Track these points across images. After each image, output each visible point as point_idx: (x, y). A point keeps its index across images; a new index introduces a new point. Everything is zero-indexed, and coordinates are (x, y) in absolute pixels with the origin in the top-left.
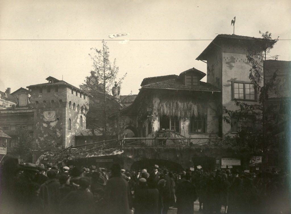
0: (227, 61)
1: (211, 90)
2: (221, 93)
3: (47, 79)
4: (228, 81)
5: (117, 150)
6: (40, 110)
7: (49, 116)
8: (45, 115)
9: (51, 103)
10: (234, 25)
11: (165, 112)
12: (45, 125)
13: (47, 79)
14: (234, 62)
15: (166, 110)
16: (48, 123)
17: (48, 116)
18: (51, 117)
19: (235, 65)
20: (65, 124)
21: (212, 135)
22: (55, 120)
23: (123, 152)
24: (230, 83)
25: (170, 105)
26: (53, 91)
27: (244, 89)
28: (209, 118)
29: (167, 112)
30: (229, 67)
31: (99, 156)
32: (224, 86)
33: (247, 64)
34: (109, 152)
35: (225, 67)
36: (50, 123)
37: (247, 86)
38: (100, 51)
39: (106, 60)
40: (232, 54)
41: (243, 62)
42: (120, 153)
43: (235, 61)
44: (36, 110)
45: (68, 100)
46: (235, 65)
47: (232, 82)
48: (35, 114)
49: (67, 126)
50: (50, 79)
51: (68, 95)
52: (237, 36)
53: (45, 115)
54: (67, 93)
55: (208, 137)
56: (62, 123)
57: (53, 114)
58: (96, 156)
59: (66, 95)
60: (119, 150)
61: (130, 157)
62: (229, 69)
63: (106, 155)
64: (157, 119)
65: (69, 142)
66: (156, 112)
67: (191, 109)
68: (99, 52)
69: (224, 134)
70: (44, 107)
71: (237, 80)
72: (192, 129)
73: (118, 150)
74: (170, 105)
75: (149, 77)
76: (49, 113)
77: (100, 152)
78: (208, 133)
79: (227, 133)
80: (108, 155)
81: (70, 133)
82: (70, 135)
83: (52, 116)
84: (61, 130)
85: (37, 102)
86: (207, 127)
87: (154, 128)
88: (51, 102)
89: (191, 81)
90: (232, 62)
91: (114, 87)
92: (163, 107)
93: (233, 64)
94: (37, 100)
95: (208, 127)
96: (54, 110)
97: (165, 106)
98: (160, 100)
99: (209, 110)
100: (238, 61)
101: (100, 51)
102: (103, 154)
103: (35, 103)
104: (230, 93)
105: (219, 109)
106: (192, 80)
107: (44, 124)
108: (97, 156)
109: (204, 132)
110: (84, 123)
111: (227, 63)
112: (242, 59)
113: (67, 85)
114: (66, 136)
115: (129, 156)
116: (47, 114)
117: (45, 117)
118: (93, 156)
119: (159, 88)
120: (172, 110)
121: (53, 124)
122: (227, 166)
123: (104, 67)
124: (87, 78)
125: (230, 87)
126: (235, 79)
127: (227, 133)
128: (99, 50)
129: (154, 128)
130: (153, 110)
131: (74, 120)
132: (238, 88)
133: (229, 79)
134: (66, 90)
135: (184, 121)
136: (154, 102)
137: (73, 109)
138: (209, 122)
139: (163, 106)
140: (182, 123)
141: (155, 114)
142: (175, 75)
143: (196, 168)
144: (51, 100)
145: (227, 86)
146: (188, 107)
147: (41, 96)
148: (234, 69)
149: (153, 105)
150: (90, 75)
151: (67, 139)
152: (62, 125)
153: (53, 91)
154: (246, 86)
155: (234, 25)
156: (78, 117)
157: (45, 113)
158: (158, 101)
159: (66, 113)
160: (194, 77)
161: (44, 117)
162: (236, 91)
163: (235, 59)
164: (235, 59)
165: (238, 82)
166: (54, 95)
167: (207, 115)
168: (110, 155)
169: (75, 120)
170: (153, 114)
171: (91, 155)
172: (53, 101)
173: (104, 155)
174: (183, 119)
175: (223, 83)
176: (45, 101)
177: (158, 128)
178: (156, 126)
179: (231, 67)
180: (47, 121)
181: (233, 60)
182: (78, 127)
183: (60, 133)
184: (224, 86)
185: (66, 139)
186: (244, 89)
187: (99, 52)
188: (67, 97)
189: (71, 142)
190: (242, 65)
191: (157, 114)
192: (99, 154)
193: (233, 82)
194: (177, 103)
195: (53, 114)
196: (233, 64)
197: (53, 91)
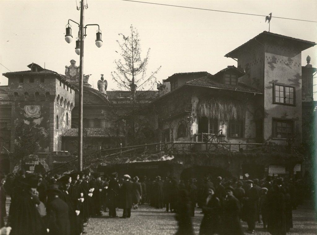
0: (269, 61)
1: (254, 92)
2: (263, 95)
3: (29, 66)
4: (270, 83)
5: (165, 155)
6: (19, 103)
7: (32, 111)
8: (27, 110)
9: (35, 96)
10: (269, 21)
11: (206, 114)
12: (26, 122)
13: (29, 66)
14: (275, 63)
15: (206, 111)
16: (31, 120)
17: (31, 112)
18: (35, 113)
19: (276, 66)
20: (53, 122)
21: (250, 141)
22: (39, 116)
23: (173, 157)
24: (272, 85)
25: (210, 106)
26: (38, 82)
27: (284, 92)
28: (247, 122)
29: (207, 113)
30: (271, 67)
31: (143, 161)
32: (266, 87)
33: (288, 66)
34: (156, 158)
35: (267, 67)
36: (33, 120)
37: (287, 89)
38: (128, 38)
39: (134, 49)
40: (274, 54)
41: (283, 63)
42: (169, 158)
43: (277, 61)
44: (14, 104)
45: (57, 93)
46: (276, 66)
47: (273, 84)
48: (13, 108)
49: (55, 124)
50: (34, 66)
51: (57, 87)
52: (272, 33)
53: (27, 110)
54: (56, 85)
55: (246, 142)
56: (48, 121)
57: (37, 108)
58: (139, 162)
59: (55, 87)
60: (167, 155)
61: (181, 163)
62: (271, 70)
63: (152, 161)
64: (196, 121)
65: (57, 144)
66: (194, 112)
67: (231, 111)
68: (126, 39)
69: (266, 140)
70: (26, 100)
71: (278, 82)
72: (230, 134)
73: (166, 155)
74: (210, 106)
75: (180, 72)
76: (32, 108)
77: (144, 157)
78: (246, 138)
79: (268, 138)
80: (155, 161)
81: (58, 133)
82: (57, 135)
83: (36, 111)
84: (48, 129)
85: (16, 94)
86: (245, 131)
87: (192, 130)
88: (34, 94)
89: (229, 80)
90: (273, 63)
91: (100, 81)
92: (203, 108)
93: (274, 65)
94: (15, 91)
95: (246, 131)
96: (37, 104)
97: (205, 106)
98: (199, 99)
99: (247, 112)
100: (279, 62)
101: (128, 38)
102: (149, 160)
103: (13, 94)
104: (271, 96)
105: (259, 114)
106: (230, 79)
107: (25, 120)
108: (141, 162)
109: (241, 136)
110: (69, 121)
111: (269, 63)
112: (282, 60)
113: (57, 75)
114: (54, 136)
115: (180, 162)
116: (29, 109)
117: (27, 112)
118: (135, 161)
119: (203, 86)
120: (213, 112)
121: (38, 122)
122: (273, 174)
123: (133, 58)
124: (66, 67)
125: (271, 90)
126: (276, 81)
127: (268, 139)
128: (126, 37)
129: (193, 131)
130: (191, 111)
131: (61, 118)
132: (279, 90)
133: (271, 81)
134: (55, 81)
135: (223, 124)
136: (192, 101)
137: (60, 104)
138: (247, 126)
139: (203, 106)
140: (220, 126)
141: (193, 114)
142: (206, 72)
143: (244, 177)
144: (35, 92)
145: (268, 88)
146: (228, 109)
147: (21, 86)
148: (275, 71)
149: (191, 104)
150: (69, 65)
151: (55, 140)
152: (49, 123)
153: (38, 82)
154: (286, 89)
155: (269, 21)
156: (64, 114)
157: (27, 108)
158: (197, 101)
159: (54, 109)
160: (232, 76)
161: (25, 113)
162: (277, 94)
163: (276, 59)
164: (276, 59)
165: (280, 85)
166: (39, 86)
167: (245, 118)
168: (158, 160)
169: (62, 117)
170: (191, 114)
171: (132, 160)
172: (37, 93)
173: (150, 161)
174: (222, 122)
175: (265, 84)
176: (26, 93)
177: (197, 130)
178: (194, 128)
179: (272, 68)
180: (29, 117)
181: (274, 60)
182: (64, 125)
183: (46, 132)
184: (266, 87)
185: (54, 139)
186: (284, 92)
187: (126, 39)
188: (56, 89)
189: (58, 143)
190: (283, 67)
191: (196, 115)
192: (143, 160)
193: (274, 84)
194: (217, 104)
195: (37, 108)
196: (274, 65)
197: (37, 81)
